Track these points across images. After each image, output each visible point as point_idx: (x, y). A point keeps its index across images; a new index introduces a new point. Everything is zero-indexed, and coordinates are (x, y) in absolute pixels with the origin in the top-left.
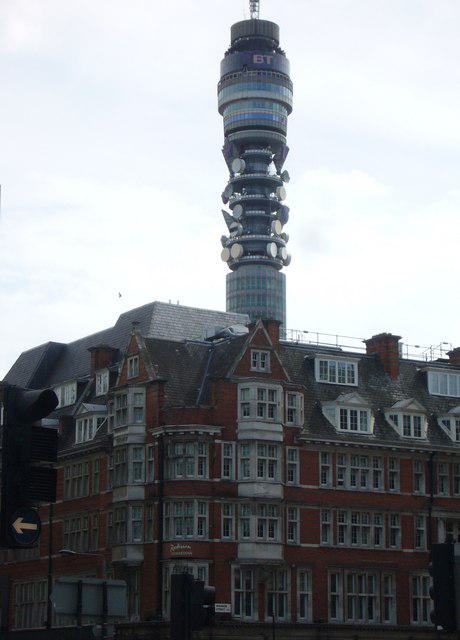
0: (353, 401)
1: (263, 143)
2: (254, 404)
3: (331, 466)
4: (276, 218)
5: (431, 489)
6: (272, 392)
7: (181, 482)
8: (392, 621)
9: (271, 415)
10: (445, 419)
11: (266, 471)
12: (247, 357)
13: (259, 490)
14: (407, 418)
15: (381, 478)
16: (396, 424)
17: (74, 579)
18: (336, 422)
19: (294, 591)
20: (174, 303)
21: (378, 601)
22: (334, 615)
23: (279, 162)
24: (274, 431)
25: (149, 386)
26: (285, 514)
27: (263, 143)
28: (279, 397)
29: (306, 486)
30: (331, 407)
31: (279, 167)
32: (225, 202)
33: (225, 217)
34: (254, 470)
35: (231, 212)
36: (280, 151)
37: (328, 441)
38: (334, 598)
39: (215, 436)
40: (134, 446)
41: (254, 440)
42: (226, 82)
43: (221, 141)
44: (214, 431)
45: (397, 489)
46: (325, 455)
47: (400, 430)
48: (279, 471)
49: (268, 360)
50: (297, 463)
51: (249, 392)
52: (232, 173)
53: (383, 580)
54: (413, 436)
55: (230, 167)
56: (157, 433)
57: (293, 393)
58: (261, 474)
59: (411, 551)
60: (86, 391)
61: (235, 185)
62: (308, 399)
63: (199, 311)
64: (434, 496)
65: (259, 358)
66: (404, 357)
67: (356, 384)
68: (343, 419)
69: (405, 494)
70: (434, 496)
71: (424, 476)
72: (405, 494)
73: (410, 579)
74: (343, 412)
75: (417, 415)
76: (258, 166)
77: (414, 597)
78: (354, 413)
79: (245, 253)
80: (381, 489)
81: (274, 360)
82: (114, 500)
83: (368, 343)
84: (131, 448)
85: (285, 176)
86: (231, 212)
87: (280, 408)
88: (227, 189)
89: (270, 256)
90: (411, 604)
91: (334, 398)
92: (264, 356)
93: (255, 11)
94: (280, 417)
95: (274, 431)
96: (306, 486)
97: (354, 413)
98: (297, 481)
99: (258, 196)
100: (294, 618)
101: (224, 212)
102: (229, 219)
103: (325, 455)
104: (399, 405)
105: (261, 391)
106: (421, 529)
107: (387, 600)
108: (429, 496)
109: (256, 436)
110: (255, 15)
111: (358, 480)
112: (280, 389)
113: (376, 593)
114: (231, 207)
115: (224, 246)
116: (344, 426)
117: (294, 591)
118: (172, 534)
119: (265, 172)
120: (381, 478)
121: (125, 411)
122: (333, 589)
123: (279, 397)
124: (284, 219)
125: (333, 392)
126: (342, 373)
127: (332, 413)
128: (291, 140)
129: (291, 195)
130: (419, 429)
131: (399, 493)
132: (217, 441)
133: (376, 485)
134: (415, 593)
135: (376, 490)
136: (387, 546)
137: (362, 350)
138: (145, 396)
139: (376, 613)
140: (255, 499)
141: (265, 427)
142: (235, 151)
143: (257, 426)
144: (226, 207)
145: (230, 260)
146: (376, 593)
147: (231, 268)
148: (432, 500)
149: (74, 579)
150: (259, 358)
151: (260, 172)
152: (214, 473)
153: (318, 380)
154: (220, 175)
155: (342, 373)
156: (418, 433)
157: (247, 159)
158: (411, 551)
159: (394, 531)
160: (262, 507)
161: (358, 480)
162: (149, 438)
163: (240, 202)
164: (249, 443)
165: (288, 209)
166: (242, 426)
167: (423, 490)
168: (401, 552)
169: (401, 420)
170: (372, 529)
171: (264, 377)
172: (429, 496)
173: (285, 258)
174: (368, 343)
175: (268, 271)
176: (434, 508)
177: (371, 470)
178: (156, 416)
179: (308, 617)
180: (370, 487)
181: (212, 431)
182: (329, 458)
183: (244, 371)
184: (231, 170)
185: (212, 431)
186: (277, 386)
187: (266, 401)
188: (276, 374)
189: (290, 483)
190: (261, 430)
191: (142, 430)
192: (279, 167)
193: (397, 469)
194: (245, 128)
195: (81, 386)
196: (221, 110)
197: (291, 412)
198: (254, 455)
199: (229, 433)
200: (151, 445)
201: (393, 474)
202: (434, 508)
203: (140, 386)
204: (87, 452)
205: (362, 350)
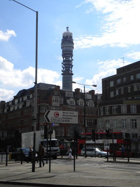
0: (72, 99)
1: (69, 54)
5: (85, 114)
6: (58, 98)
7: (42, 113)
12: (54, 92)
14: (81, 102)
17: (2, 131)
18: (69, 103)
19: (61, 131)
20: (44, 83)
22: (68, 135)
23: (72, 57)
24: (58, 105)
27: (69, 54)
28: (59, 99)
31: (71, 58)
36: (72, 55)
38: (68, 132)
42: (62, 44)
43: (62, 53)
47: (79, 104)
49: (57, 93)
51: (54, 98)
56: (39, 105)
60: (28, 98)
61: (64, 61)
62: (64, 99)
63: (29, 89)
65: (56, 92)
68: (70, 102)
74: (70, 101)
76: (68, 58)
78: (72, 101)
81: (58, 93)
82: (32, 116)
85: (72, 60)
91: (69, 99)
92: (57, 92)
95: (58, 105)
97: (72, 101)
100: (61, 135)
102: (63, 68)
104: (79, 100)
109: (55, 105)
112: (59, 97)
116: (70, 104)
117: (61, 131)
118: (41, 122)
119: (69, 59)
121: (34, 101)
122: (68, 131)
123: (59, 99)
125: (69, 98)
126: (70, 95)
127: (68, 101)
128: (73, 53)
129: (74, 63)
142: (64, 55)
143: (55, 104)
144: (62, 65)
149: (2, 131)
150: (56, 92)
153: (66, 96)
154: (61, 59)
155: (70, 95)
169: (80, 102)
171: (57, 95)
175: (69, 76)
178: (39, 102)
179: (63, 135)
183: (53, 94)
185: (48, 104)
188: (58, 95)
192: (71, 58)
194: (67, 51)
195: (28, 97)
199: (51, 105)
204: (28, 108)
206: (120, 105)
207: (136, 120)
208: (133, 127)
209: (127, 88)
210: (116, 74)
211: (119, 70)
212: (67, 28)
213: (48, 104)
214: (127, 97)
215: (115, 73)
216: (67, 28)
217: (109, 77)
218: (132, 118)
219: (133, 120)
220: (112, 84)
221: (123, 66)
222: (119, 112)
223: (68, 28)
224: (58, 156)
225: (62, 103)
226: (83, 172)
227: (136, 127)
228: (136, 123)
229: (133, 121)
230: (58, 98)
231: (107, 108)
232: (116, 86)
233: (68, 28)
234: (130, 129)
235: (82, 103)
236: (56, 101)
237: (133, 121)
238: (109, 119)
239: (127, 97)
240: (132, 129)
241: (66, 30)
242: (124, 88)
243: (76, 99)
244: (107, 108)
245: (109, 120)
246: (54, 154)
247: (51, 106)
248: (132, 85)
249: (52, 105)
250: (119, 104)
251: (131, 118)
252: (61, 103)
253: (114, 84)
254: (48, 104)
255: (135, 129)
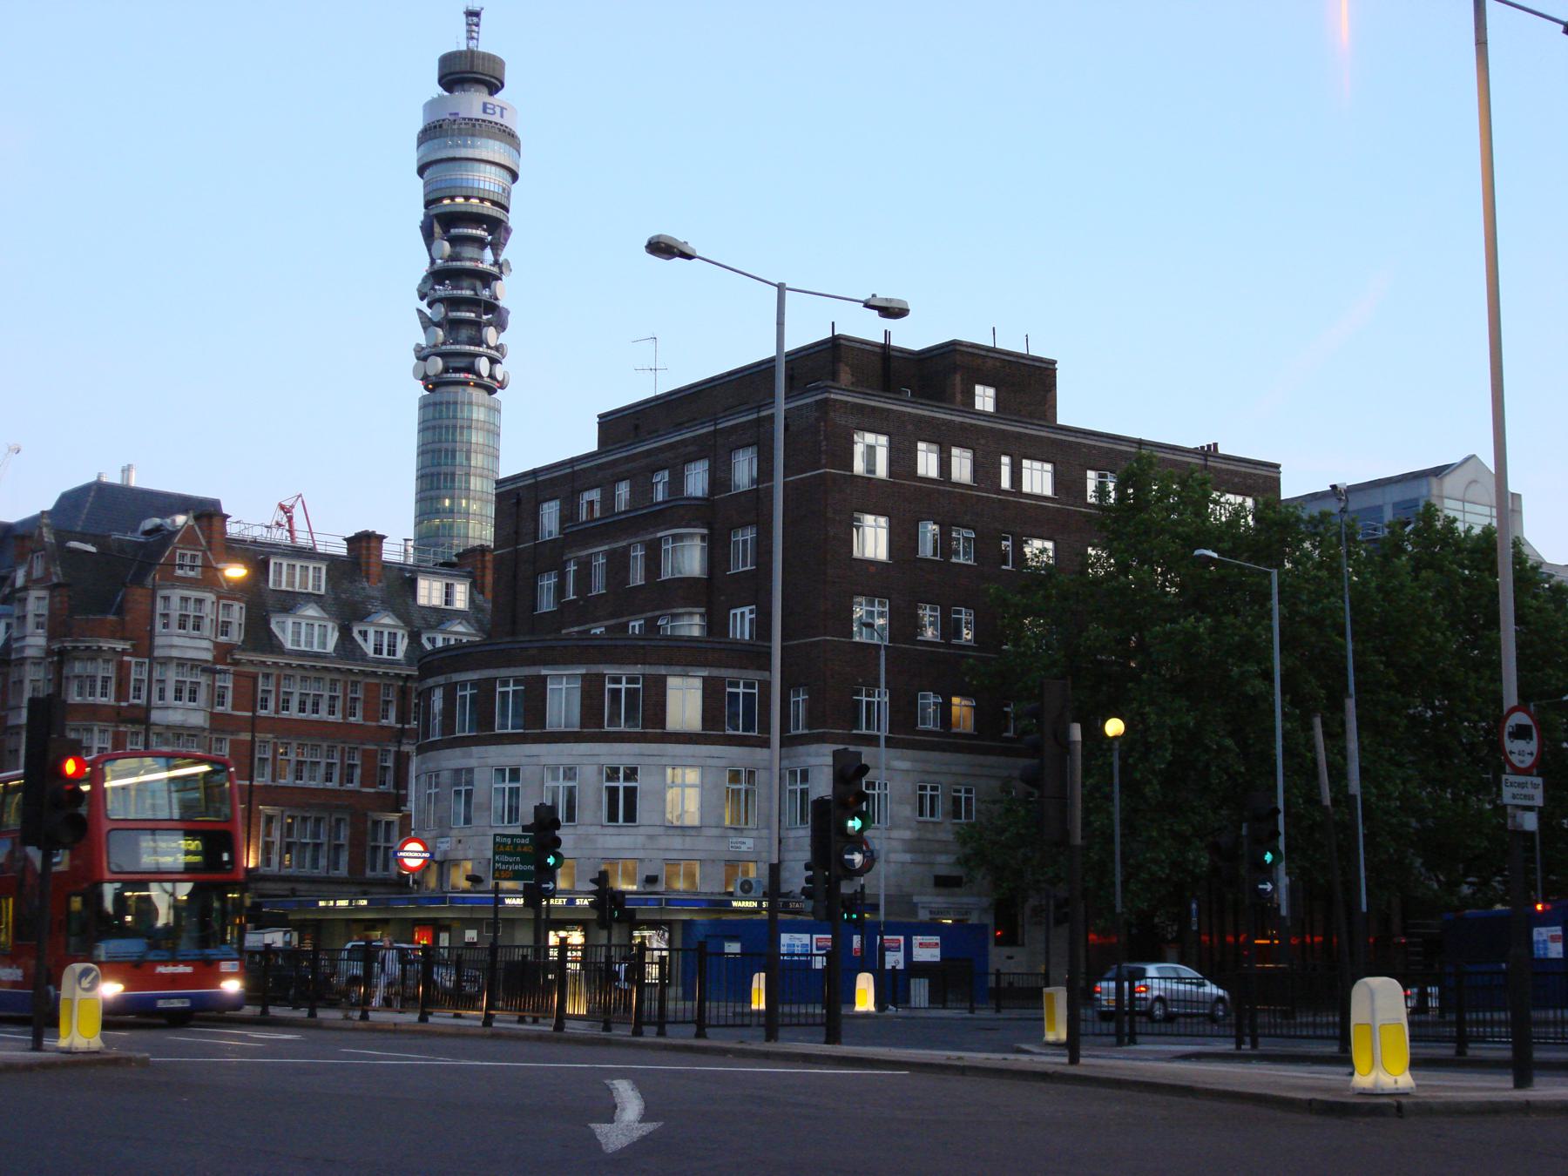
2: (175, 613)
3: (273, 688)
4: (489, 324)
5: (402, 717)
6: (200, 601)
8: (343, 871)
9: (197, 627)
10: (431, 635)
11: (186, 695)
13: (175, 717)
15: (339, 704)
16: (366, 640)
21: (325, 848)
23: (497, 247)
25: (53, 588)
26: (210, 746)
29: (239, 713)
30: (280, 620)
31: (496, 255)
32: (422, 298)
33: (420, 318)
34: (170, 693)
35: (428, 311)
37: (270, 659)
39: (124, 652)
40: (31, 660)
41: (171, 658)
44: (122, 647)
45: (357, 719)
46: (267, 676)
47: (369, 649)
48: (203, 694)
50: (230, 685)
52: (433, 261)
53: (333, 823)
54: (385, 655)
55: (429, 250)
57: (230, 602)
58: (178, 697)
59: (372, 790)
61: (437, 276)
64: (407, 726)
65: (187, 561)
66: (1048, 467)
67: (323, 591)
69: (369, 723)
70: (407, 726)
71: (395, 703)
72: (369, 723)
73: (369, 824)
75: (392, 630)
77: (372, 844)
79: (446, 370)
80: (337, 718)
83: (349, 541)
84: (29, 661)
86: (428, 311)
87: (207, 621)
88: (425, 280)
89: (479, 375)
90: (368, 854)
92: (194, 557)
93: (472, 38)
94: (207, 629)
96: (239, 713)
98: (227, 708)
99: (468, 293)
101: (420, 311)
102: (427, 323)
103: (267, 676)
105: (185, 599)
106: (387, 764)
107: (338, 847)
108: (399, 726)
109: (175, 653)
110: (472, 44)
111: (309, 707)
113: (323, 839)
114: (430, 305)
115: (418, 358)
120: (339, 704)
123: (208, 609)
124: (501, 326)
125: (289, 602)
127: (286, 630)
130: (394, 646)
131: (361, 722)
132: (126, 658)
133: (332, 712)
134: (375, 839)
135: (331, 718)
136: (341, 785)
137: (342, 550)
138: (47, 601)
139: (323, 862)
140: (168, 727)
141: (188, 642)
142: (437, 229)
144: (423, 305)
145: (425, 378)
146: (323, 839)
147: (426, 388)
148: (402, 730)
151: (471, 259)
152: (121, 693)
156: (392, 652)
157: (454, 241)
158: (372, 790)
159: (353, 766)
160: (178, 736)
161: (309, 707)
162: (49, 652)
163: (441, 300)
164: (166, 661)
165: (508, 313)
166: (158, 641)
167: (391, 720)
168: (359, 792)
170: (323, 765)
172: (399, 726)
173: (500, 378)
174: (349, 541)
176: (405, 741)
177: (326, 694)
180: (323, 715)
181: (119, 646)
182: (273, 680)
184: (430, 255)
185: (119, 646)
186: (207, 595)
187: (191, 610)
189: (219, 709)
190: (182, 647)
191: (42, 641)
192: (496, 255)
193: (360, 694)
196: (421, 171)
197: (226, 624)
198: (172, 676)
199: (144, 646)
200: (50, 660)
201: (354, 700)
202: (405, 741)
203: (42, 589)
205: (342, 550)
206: (544, 672)
207: (631, 773)
208: (613, 817)
209: (625, 553)
210: (592, 446)
211: (615, 426)
212: (473, 14)
213: (127, 646)
214: (624, 620)
215: (588, 442)
216: (473, 14)
217: (534, 473)
218: (614, 761)
219: (613, 773)
220: (550, 516)
221: (650, 394)
222: (534, 726)
223: (477, 14)
224: (1114, 906)
225: (236, 636)
226: (1201, 1019)
227: (630, 816)
228: (631, 794)
229: (627, 778)
230: (200, 601)
231: (468, 693)
232: (576, 534)
233: (477, 14)
234: (593, 830)
235: (393, 636)
236: (182, 626)
237: (627, 778)
238: (472, 763)
239: (624, 620)
240: (611, 830)
241: (464, 34)
242: (609, 555)
243: (348, 614)
244: (468, 693)
245: (470, 771)
246: (186, 1004)
247: (153, 659)
248: (652, 536)
249: (157, 653)
250: (534, 664)
251: (603, 760)
252: (222, 639)
253: (563, 520)
254: (127, 646)
255: (623, 830)
